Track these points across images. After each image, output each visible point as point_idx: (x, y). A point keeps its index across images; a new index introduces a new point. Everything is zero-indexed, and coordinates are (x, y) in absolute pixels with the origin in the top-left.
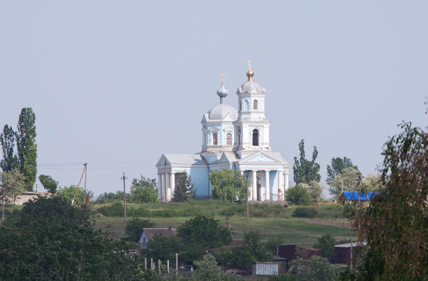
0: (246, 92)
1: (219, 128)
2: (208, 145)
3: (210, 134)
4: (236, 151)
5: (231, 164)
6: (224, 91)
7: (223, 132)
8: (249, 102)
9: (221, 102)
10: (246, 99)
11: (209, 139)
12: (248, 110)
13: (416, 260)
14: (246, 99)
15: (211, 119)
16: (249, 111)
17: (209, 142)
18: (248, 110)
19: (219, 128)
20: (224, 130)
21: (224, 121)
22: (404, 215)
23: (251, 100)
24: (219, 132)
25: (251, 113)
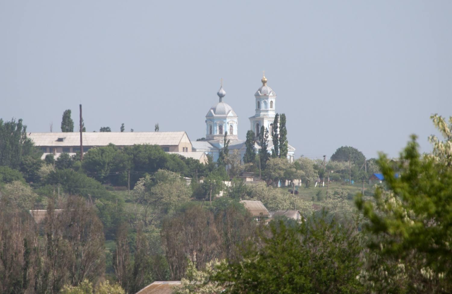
0: (265, 95)
1: (224, 121)
2: (215, 134)
3: (216, 126)
4: (372, 201)
5: (247, 165)
6: (223, 92)
7: (227, 124)
8: (267, 102)
9: (220, 101)
10: (265, 100)
11: (215, 129)
12: (266, 108)
13: (20, 234)
14: (265, 100)
15: (217, 114)
16: (267, 109)
17: (215, 132)
18: (266, 108)
19: (224, 121)
20: (228, 123)
21: (228, 116)
22: (178, 178)
23: (270, 100)
24: (224, 124)
25: (269, 111)
